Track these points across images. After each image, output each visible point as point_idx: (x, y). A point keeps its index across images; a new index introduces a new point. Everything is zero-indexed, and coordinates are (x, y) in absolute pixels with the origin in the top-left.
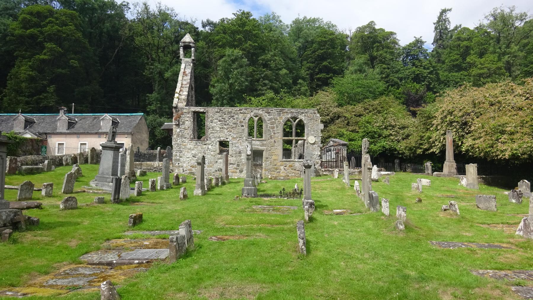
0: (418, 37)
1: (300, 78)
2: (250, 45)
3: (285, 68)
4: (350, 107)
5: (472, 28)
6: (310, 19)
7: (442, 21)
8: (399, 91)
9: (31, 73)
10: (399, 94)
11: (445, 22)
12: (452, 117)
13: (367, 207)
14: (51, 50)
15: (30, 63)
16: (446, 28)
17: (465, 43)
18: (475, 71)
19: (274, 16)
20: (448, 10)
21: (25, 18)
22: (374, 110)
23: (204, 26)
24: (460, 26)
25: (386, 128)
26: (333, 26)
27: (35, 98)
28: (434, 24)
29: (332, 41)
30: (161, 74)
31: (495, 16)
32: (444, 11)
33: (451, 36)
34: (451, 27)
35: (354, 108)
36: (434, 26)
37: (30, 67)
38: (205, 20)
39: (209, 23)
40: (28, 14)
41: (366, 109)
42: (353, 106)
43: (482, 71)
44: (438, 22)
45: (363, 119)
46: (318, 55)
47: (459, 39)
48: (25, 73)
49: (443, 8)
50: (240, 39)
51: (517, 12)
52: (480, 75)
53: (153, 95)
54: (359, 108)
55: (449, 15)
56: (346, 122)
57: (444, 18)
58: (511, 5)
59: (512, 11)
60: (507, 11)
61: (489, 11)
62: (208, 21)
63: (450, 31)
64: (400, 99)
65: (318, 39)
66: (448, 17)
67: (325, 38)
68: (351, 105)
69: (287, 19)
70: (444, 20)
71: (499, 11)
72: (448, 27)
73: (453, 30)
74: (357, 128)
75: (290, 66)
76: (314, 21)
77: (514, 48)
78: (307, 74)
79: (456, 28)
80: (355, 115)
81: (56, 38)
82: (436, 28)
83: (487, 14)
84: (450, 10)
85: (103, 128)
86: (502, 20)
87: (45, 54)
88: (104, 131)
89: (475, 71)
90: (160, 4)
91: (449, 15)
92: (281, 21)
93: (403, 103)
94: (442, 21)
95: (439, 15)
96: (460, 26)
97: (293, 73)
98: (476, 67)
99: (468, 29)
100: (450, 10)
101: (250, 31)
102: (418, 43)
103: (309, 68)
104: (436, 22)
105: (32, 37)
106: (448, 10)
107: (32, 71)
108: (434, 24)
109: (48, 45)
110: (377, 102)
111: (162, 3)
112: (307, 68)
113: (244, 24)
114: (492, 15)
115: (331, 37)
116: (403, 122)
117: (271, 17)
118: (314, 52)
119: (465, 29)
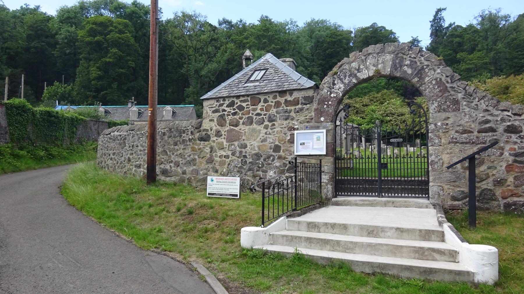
0: (415, 37)
1: (313, 74)
2: (274, 48)
3: (302, 66)
4: (358, 99)
5: (464, 26)
6: (318, 21)
7: (437, 20)
8: (398, 84)
9: (99, 73)
10: (398, 86)
11: (440, 20)
12: (185, 168)
13: (406, 110)
14: (115, 53)
15: (98, 65)
16: (441, 26)
17: (458, 39)
18: (463, 66)
19: (292, 21)
20: (443, 9)
21: (92, 28)
22: (377, 101)
23: (220, 24)
24: (454, 23)
25: (387, 115)
26: (340, 27)
27: (102, 93)
28: (431, 22)
29: (340, 41)
30: (197, 72)
31: (483, 17)
32: (439, 10)
33: (446, 33)
34: (446, 25)
35: (361, 100)
36: (430, 24)
37: (98, 68)
38: (221, 19)
39: (225, 22)
40: (93, 24)
41: (371, 100)
42: (360, 98)
43: (470, 66)
44: (434, 20)
45: (370, 107)
46: (328, 54)
47: (452, 35)
48: (95, 73)
49: (438, 8)
50: (265, 43)
51: (502, 13)
52: (469, 70)
53: (190, 89)
54: (366, 100)
55: (443, 14)
56: (355, 111)
57: (439, 16)
58: (497, 8)
59: (498, 12)
60: (494, 12)
61: (477, 12)
62: (224, 19)
63: (445, 28)
64: (399, 91)
65: (328, 40)
66: (443, 15)
67: (334, 38)
68: (359, 97)
69: (301, 22)
70: (440, 18)
71: (487, 12)
72: (443, 25)
73: (448, 28)
74: (364, 116)
75: (306, 65)
76: (323, 22)
77: (500, 45)
78: (320, 70)
79: (451, 25)
80: (363, 105)
81: (116, 44)
82: (432, 26)
83: (476, 15)
84: (445, 9)
85: (165, 116)
86: (491, 21)
87: (110, 57)
88: (167, 119)
89: (463, 66)
90: (194, 12)
91: (443, 14)
92: (297, 26)
93: (402, 95)
94: (437, 20)
95: (434, 13)
96: (454, 23)
97: (309, 70)
98: (465, 62)
99: (461, 27)
100: (445, 9)
101: (273, 36)
102: (414, 42)
103: (321, 65)
104: (432, 20)
105: (98, 43)
106: (443, 9)
107: (100, 71)
108: (431, 22)
109: (115, 50)
110: (379, 95)
111: (196, 12)
112: (319, 64)
113: (267, 30)
114: (481, 16)
115: (339, 38)
116: (400, 110)
117: (290, 22)
118: (325, 51)
119: (458, 26)
